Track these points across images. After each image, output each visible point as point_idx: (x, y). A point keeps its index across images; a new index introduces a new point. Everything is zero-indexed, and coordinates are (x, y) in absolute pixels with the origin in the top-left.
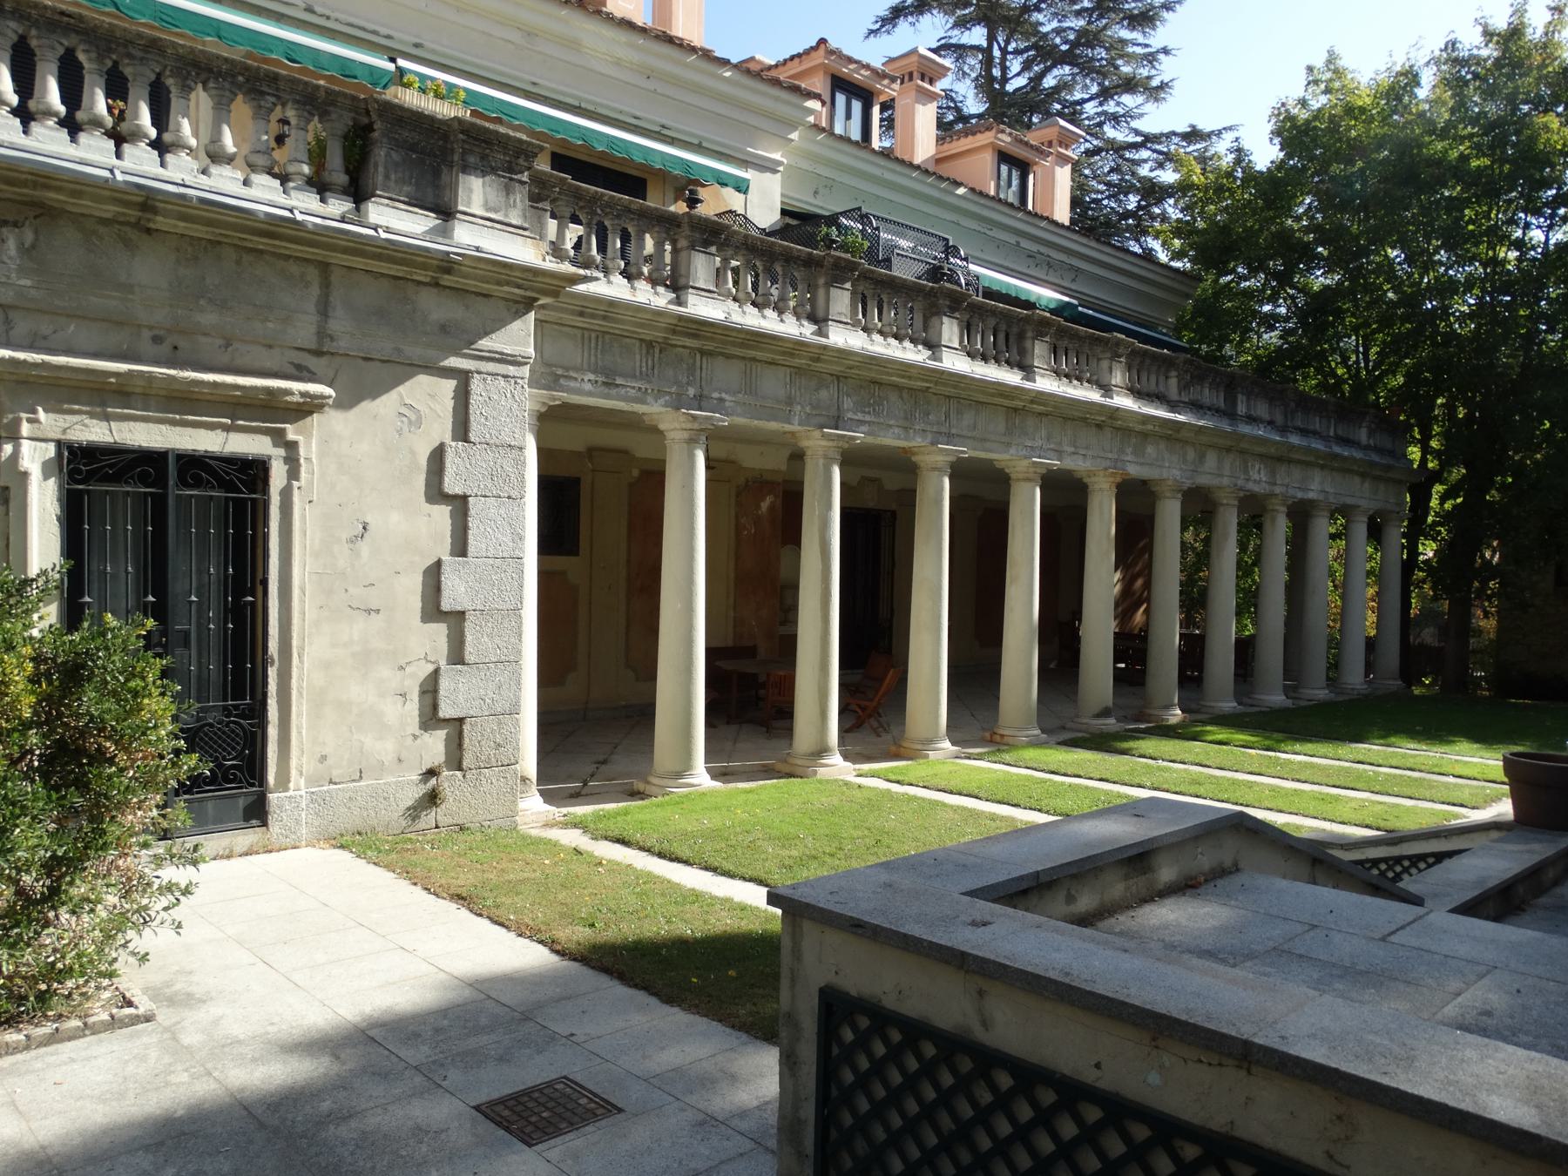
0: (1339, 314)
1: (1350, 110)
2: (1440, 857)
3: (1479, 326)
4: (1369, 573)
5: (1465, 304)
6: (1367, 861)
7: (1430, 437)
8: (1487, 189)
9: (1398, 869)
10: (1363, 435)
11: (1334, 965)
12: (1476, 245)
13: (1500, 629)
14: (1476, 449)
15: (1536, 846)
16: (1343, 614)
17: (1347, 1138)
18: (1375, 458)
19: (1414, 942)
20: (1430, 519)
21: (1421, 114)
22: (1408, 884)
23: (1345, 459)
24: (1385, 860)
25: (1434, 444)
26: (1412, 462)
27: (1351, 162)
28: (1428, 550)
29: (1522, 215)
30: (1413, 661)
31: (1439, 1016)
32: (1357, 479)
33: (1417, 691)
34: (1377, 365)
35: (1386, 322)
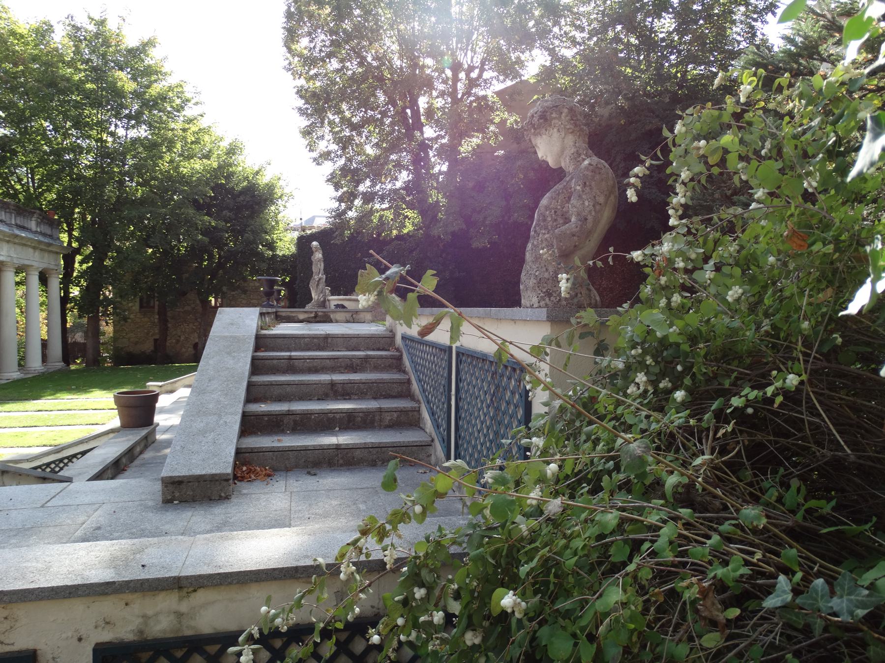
0: (14, 153)
1: (13, 33)
2: (84, 453)
3: (96, 173)
4: (42, 304)
5: (86, 160)
6: (44, 465)
7: (73, 230)
8: (96, 102)
9: (61, 465)
10: (33, 225)
11: (11, 530)
12: (92, 129)
13: (115, 331)
14: (98, 236)
15: (130, 437)
16: (26, 330)
17: (11, 627)
18: (41, 238)
19: (61, 503)
20: (75, 274)
21: (56, 49)
22: (65, 473)
23: (23, 238)
24: (54, 462)
25: (75, 233)
26: (63, 242)
27: (16, 65)
28: (75, 291)
29: (114, 120)
30: (69, 352)
31: (73, 538)
32: (31, 250)
33: (73, 367)
34: (39, 187)
35: (43, 163)
